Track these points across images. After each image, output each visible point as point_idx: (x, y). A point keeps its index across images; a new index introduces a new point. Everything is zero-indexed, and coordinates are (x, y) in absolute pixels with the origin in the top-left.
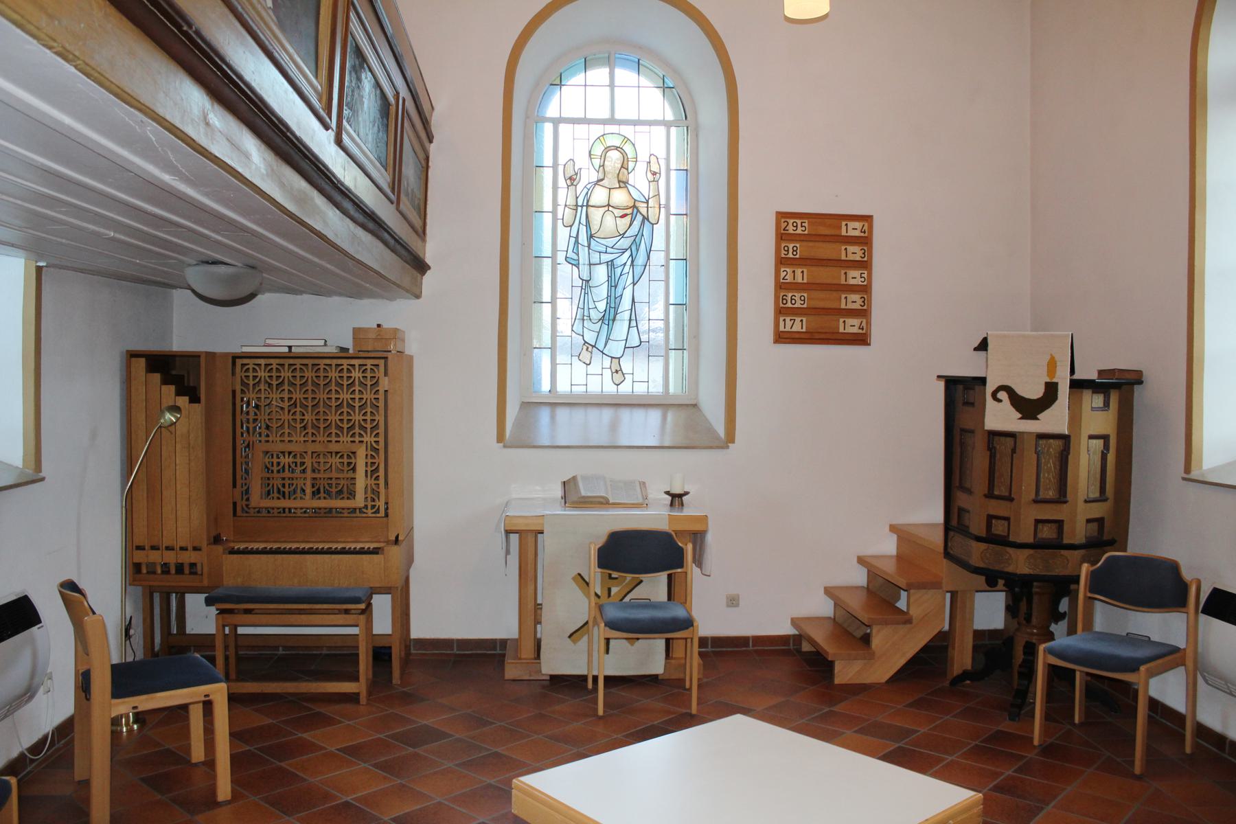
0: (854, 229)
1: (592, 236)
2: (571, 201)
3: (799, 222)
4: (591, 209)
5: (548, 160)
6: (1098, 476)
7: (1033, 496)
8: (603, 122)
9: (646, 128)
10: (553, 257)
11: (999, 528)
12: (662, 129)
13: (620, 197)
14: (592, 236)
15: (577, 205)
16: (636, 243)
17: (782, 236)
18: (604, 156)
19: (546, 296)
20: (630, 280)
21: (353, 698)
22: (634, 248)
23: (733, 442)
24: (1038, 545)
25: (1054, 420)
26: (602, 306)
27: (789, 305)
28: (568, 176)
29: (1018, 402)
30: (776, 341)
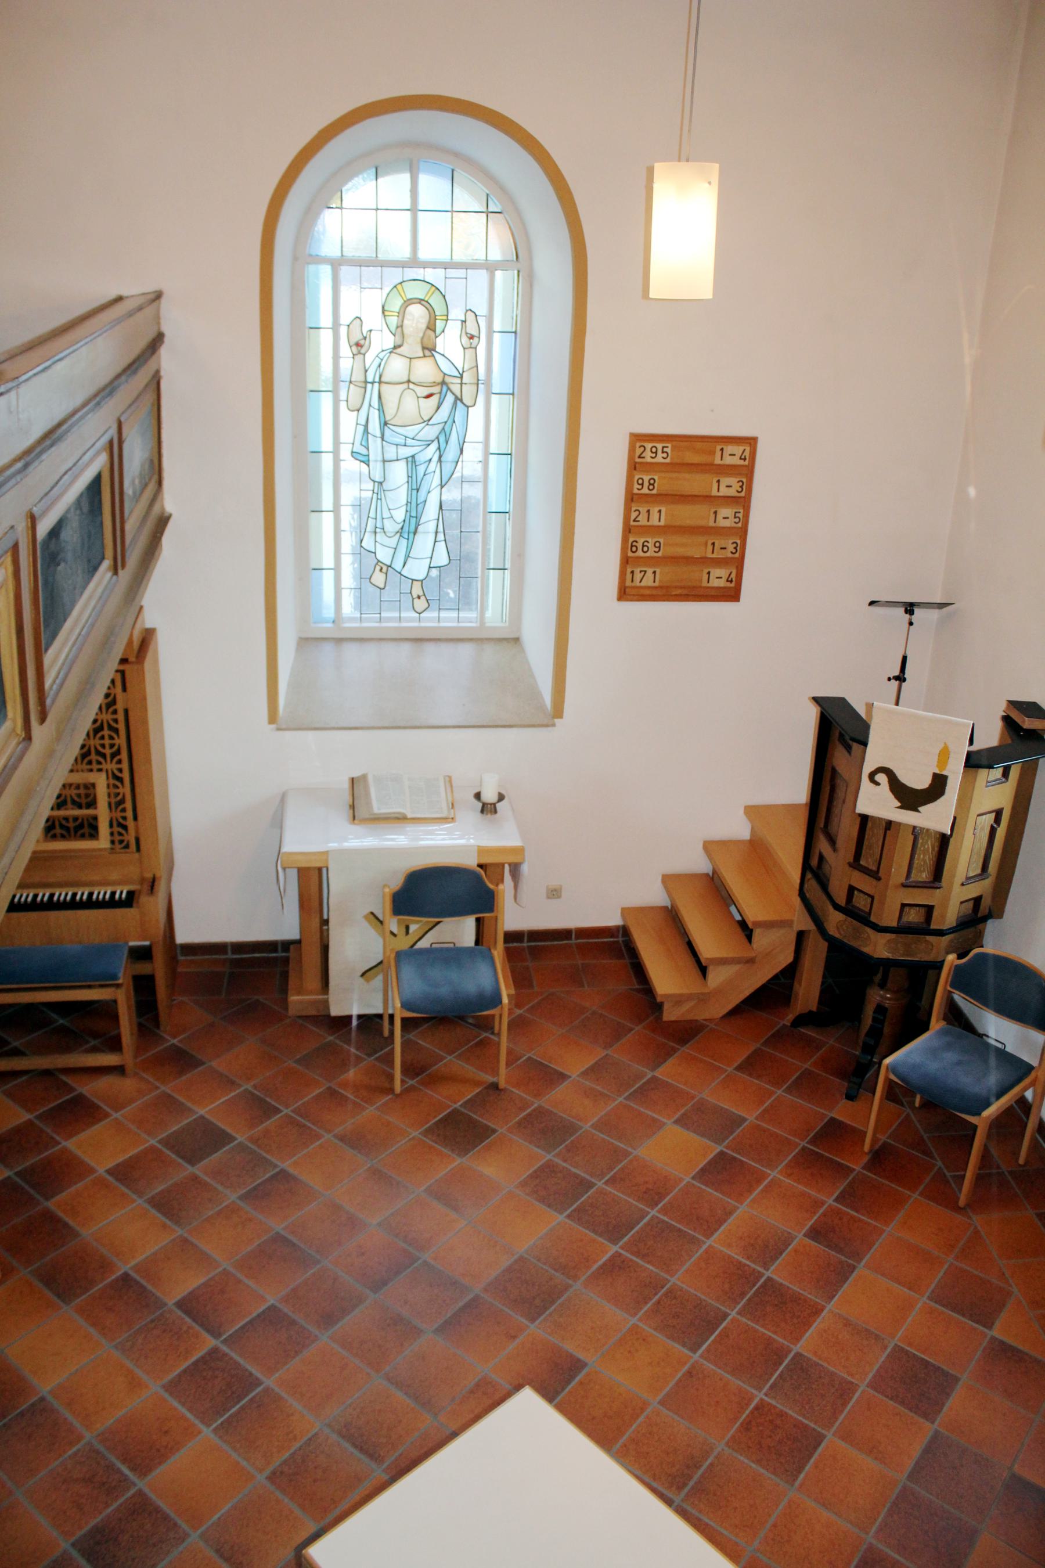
0: (732, 456)
1: (386, 424)
2: (358, 376)
3: (660, 446)
4: (384, 387)
5: (325, 318)
6: (983, 852)
7: (903, 880)
8: (402, 265)
9: (461, 273)
10: (336, 452)
11: (860, 902)
12: (483, 274)
13: (424, 370)
14: (386, 424)
15: (366, 382)
16: (444, 434)
17: (634, 466)
18: (402, 313)
19: (327, 503)
20: (436, 481)
21: (119, 1070)
22: (442, 439)
23: (561, 717)
24: (902, 930)
25: (934, 817)
26: (400, 515)
27: (640, 553)
28: (353, 341)
29: (898, 788)
30: (620, 598)
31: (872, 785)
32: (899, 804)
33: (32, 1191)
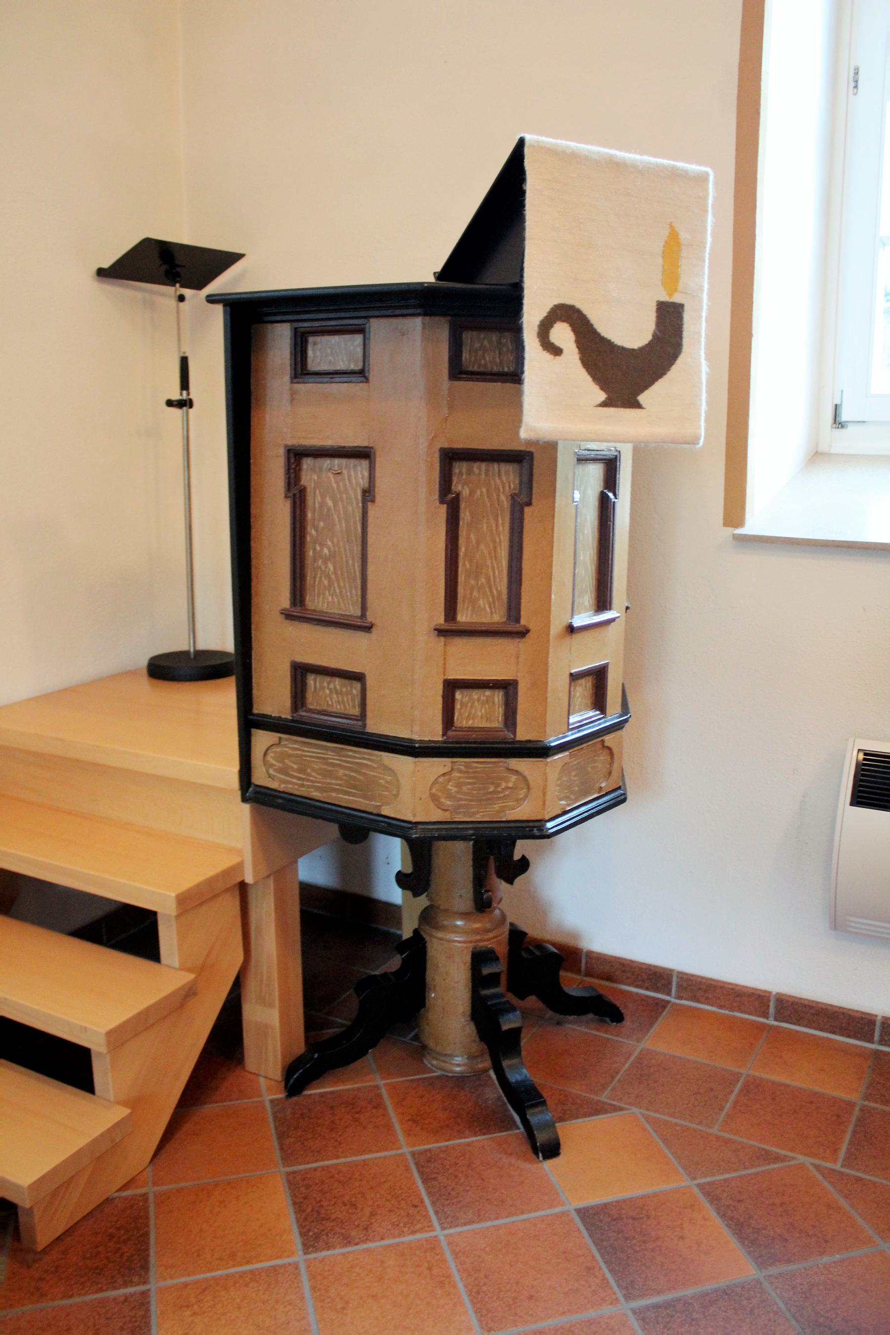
31: (547, 356)
32: (602, 396)
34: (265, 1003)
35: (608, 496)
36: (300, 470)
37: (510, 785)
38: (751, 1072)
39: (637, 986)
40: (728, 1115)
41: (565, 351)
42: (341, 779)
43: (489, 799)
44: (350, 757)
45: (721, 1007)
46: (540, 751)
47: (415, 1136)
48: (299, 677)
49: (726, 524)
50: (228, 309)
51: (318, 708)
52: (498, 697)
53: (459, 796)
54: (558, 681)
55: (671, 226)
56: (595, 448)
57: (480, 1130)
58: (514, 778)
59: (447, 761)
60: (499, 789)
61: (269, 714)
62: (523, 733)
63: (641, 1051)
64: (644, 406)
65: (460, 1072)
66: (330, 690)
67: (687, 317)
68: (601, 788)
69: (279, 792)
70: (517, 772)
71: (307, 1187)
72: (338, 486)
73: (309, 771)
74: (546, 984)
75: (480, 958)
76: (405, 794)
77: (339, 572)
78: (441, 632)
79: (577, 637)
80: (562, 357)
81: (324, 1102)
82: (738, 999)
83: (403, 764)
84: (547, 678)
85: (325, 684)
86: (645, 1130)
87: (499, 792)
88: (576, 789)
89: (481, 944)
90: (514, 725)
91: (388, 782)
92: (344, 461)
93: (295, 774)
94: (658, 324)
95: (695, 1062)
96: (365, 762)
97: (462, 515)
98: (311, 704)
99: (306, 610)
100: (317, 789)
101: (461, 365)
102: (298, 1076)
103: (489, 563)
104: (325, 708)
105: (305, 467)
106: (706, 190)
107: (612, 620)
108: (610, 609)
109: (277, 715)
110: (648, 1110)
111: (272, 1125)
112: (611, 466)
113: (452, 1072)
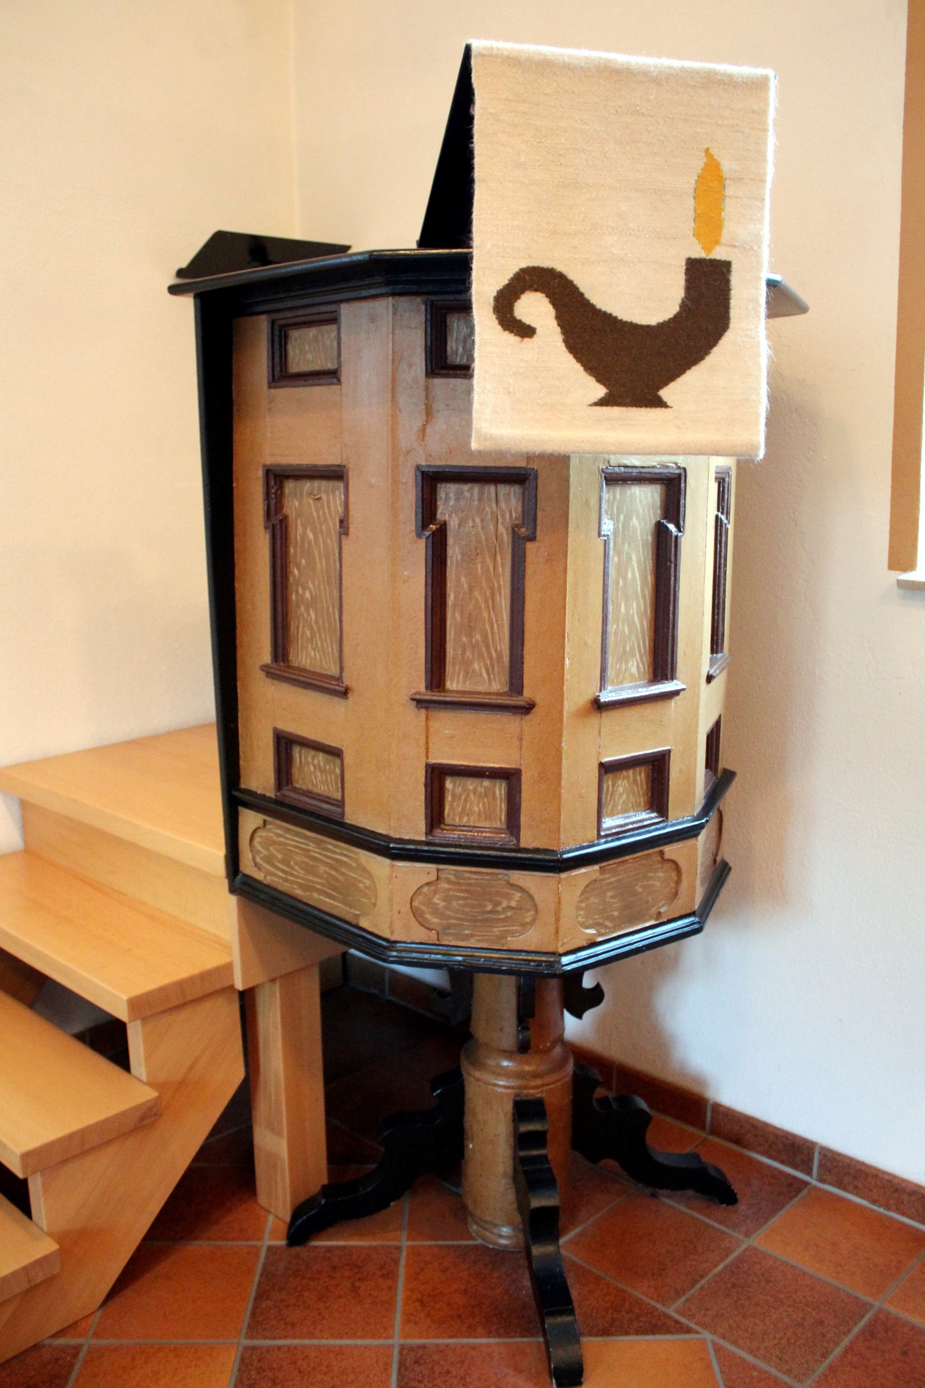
31: (511, 339)
32: (600, 391)
33: (722, 1228)
34: (274, 1129)
35: (667, 528)
36: (282, 494)
37: (513, 904)
38: (886, 1307)
39: (771, 1157)
40: (831, 1368)
41: (538, 331)
42: (322, 878)
43: (486, 920)
44: (330, 851)
45: (874, 1202)
46: (553, 864)
47: (416, 1323)
48: (283, 749)
49: (891, 567)
50: (198, 300)
51: (304, 787)
52: (500, 789)
53: (448, 913)
54: (578, 775)
55: (707, 151)
56: (637, 463)
57: (497, 1330)
58: (518, 895)
59: (432, 867)
60: (499, 908)
61: (254, 790)
62: (529, 839)
63: (746, 1249)
64: (668, 404)
65: (506, 1246)
66: (315, 766)
67: (736, 279)
68: (660, 913)
69: (265, 885)
70: (521, 889)
71: (260, 1370)
72: (318, 514)
73: (292, 863)
74: (646, 1141)
75: (525, 1109)
76: (383, 906)
77: (321, 622)
78: (420, 703)
79: (609, 718)
80: (536, 338)
81: (329, 1259)
82: (896, 1195)
83: (379, 865)
84: (560, 769)
85: (310, 759)
86: (709, 1366)
87: (498, 912)
88: (616, 914)
89: (525, 1092)
90: (518, 827)
91: (366, 887)
92: (324, 484)
93: (280, 865)
94: (688, 289)
95: (811, 1277)
96: (345, 859)
97: (450, 552)
98: (298, 782)
99: (289, 667)
100: (301, 886)
101: (446, 358)
102: (307, 1223)
103: (485, 614)
104: (310, 787)
105: (287, 491)
106: (766, 101)
107: (676, 693)
108: (672, 678)
109: (263, 793)
110: (724, 1338)
111: (257, 1278)
112: (672, 487)
113: (496, 1244)
